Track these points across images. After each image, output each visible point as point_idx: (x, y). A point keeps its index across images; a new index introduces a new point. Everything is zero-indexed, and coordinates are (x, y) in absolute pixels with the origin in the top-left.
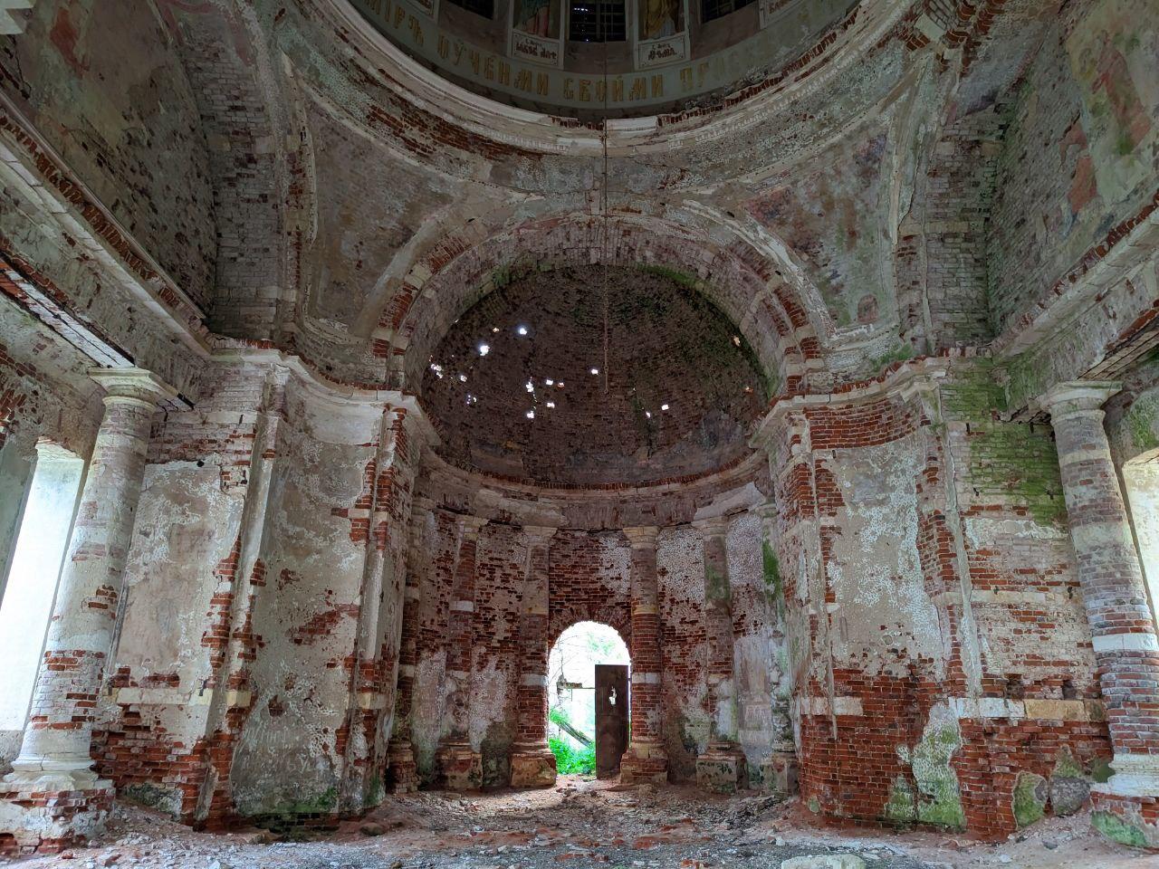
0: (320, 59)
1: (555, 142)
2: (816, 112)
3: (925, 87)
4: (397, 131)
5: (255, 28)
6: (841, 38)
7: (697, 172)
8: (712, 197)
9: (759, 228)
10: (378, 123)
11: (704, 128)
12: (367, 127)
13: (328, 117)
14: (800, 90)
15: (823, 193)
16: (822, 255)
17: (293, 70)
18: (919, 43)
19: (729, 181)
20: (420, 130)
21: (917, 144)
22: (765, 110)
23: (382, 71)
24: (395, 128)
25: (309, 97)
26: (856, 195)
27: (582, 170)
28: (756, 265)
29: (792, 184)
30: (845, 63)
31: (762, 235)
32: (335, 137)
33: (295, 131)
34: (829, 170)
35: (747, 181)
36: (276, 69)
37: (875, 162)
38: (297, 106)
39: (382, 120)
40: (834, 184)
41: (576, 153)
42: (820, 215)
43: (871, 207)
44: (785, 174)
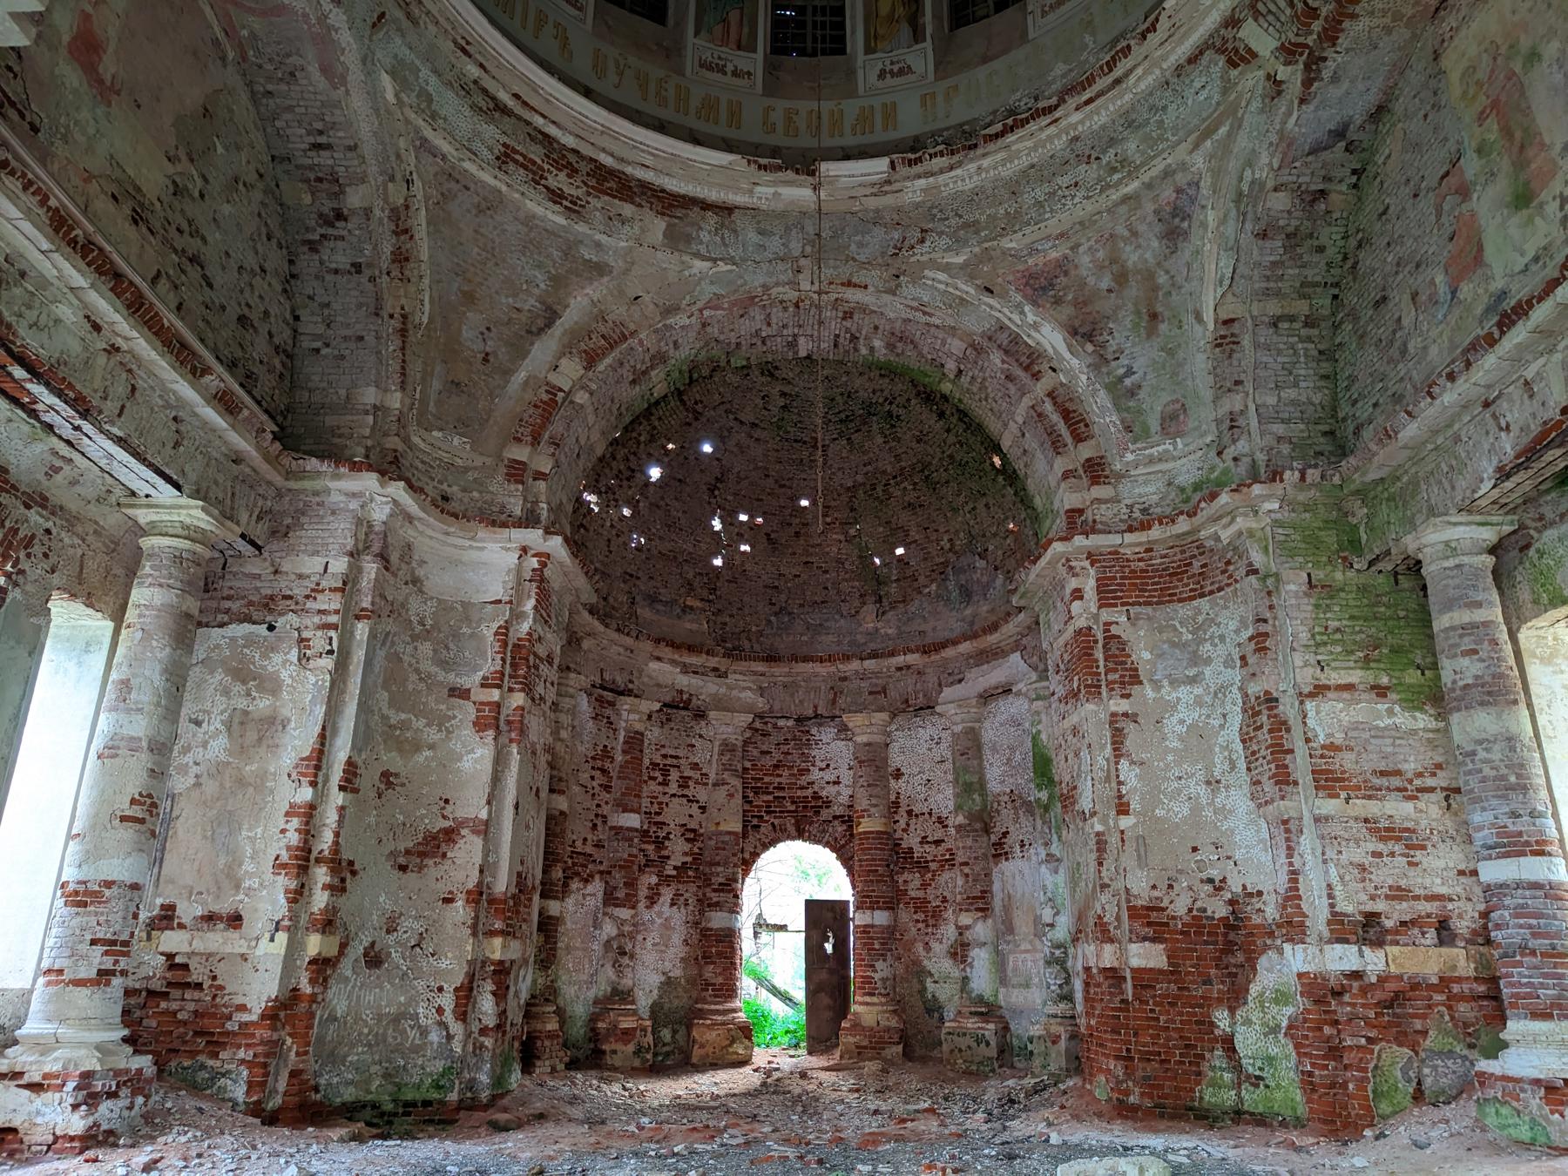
0: (433, 80)
1: (751, 192)
2: (1104, 152)
3: (1252, 116)
4: (537, 177)
5: (345, 37)
6: (1138, 51)
7: (943, 233)
8: (965, 265)
9: (1027, 309)
10: (512, 166)
11: (953, 173)
12: (497, 172)
13: (444, 158)
14: (1082, 122)
15: (1113, 261)
16: (1113, 345)
17: (396, 95)
18: (1243, 59)
19: (986, 245)
20: (569, 176)
21: (1240, 194)
22: (1035, 148)
23: (516, 96)
24: (534, 173)
25: (417, 130)
26: (1159, 264)
27: (788, 229)
28: (1023, 359)
29: (1072, 249)
30: (1143, 86)
31: (1031, 318)
32: (453, 185)
33: (398, 177)
34: (1121, 230)
35: (1013, 245)
36: (374, 94)
37: (1183, 219)
38: (402, 143)
39: (516, 162)
40: (1128, 248)
41: (780, 207)
42: (1110, 291)
43: (1179, 279)
44: (1062, 235)
